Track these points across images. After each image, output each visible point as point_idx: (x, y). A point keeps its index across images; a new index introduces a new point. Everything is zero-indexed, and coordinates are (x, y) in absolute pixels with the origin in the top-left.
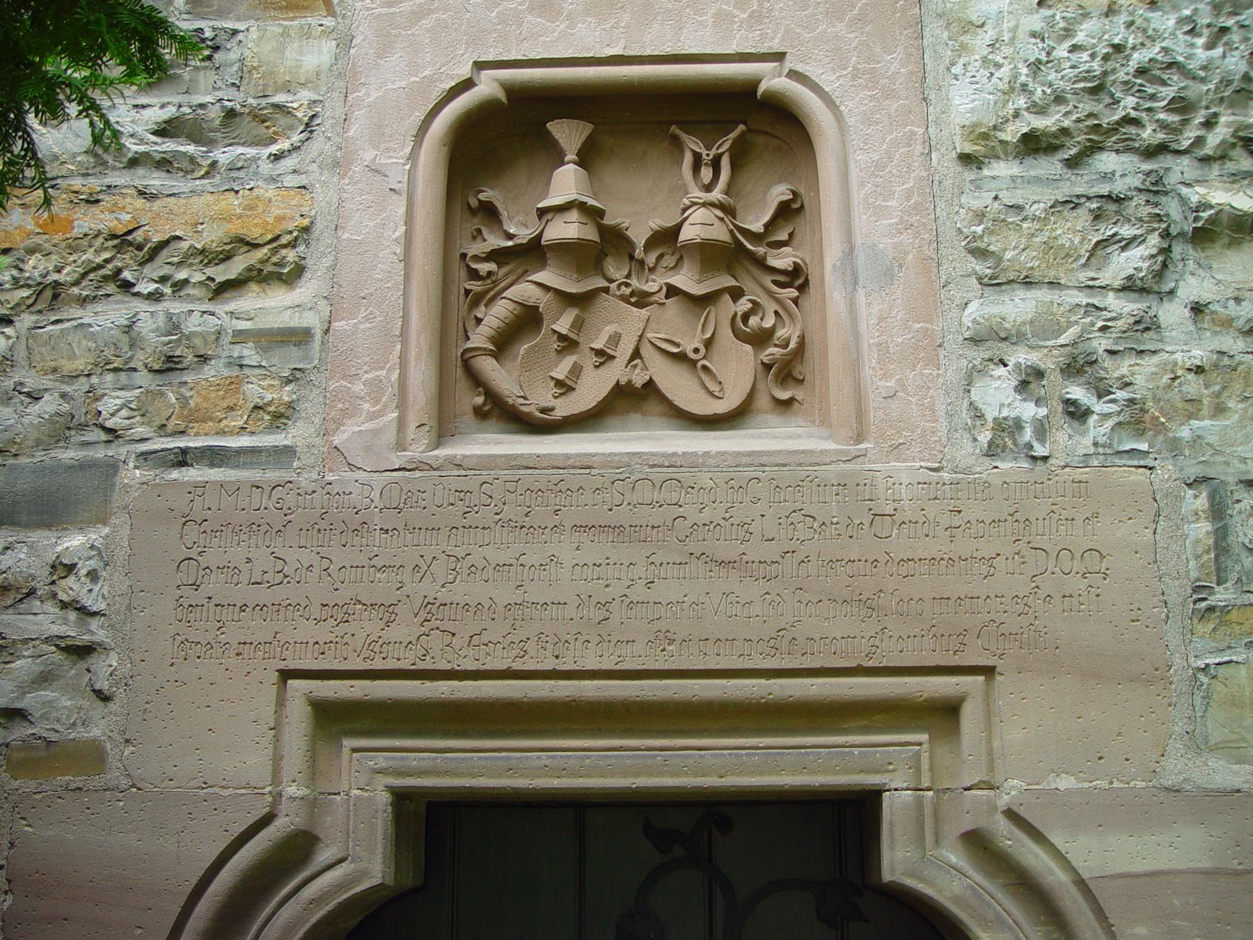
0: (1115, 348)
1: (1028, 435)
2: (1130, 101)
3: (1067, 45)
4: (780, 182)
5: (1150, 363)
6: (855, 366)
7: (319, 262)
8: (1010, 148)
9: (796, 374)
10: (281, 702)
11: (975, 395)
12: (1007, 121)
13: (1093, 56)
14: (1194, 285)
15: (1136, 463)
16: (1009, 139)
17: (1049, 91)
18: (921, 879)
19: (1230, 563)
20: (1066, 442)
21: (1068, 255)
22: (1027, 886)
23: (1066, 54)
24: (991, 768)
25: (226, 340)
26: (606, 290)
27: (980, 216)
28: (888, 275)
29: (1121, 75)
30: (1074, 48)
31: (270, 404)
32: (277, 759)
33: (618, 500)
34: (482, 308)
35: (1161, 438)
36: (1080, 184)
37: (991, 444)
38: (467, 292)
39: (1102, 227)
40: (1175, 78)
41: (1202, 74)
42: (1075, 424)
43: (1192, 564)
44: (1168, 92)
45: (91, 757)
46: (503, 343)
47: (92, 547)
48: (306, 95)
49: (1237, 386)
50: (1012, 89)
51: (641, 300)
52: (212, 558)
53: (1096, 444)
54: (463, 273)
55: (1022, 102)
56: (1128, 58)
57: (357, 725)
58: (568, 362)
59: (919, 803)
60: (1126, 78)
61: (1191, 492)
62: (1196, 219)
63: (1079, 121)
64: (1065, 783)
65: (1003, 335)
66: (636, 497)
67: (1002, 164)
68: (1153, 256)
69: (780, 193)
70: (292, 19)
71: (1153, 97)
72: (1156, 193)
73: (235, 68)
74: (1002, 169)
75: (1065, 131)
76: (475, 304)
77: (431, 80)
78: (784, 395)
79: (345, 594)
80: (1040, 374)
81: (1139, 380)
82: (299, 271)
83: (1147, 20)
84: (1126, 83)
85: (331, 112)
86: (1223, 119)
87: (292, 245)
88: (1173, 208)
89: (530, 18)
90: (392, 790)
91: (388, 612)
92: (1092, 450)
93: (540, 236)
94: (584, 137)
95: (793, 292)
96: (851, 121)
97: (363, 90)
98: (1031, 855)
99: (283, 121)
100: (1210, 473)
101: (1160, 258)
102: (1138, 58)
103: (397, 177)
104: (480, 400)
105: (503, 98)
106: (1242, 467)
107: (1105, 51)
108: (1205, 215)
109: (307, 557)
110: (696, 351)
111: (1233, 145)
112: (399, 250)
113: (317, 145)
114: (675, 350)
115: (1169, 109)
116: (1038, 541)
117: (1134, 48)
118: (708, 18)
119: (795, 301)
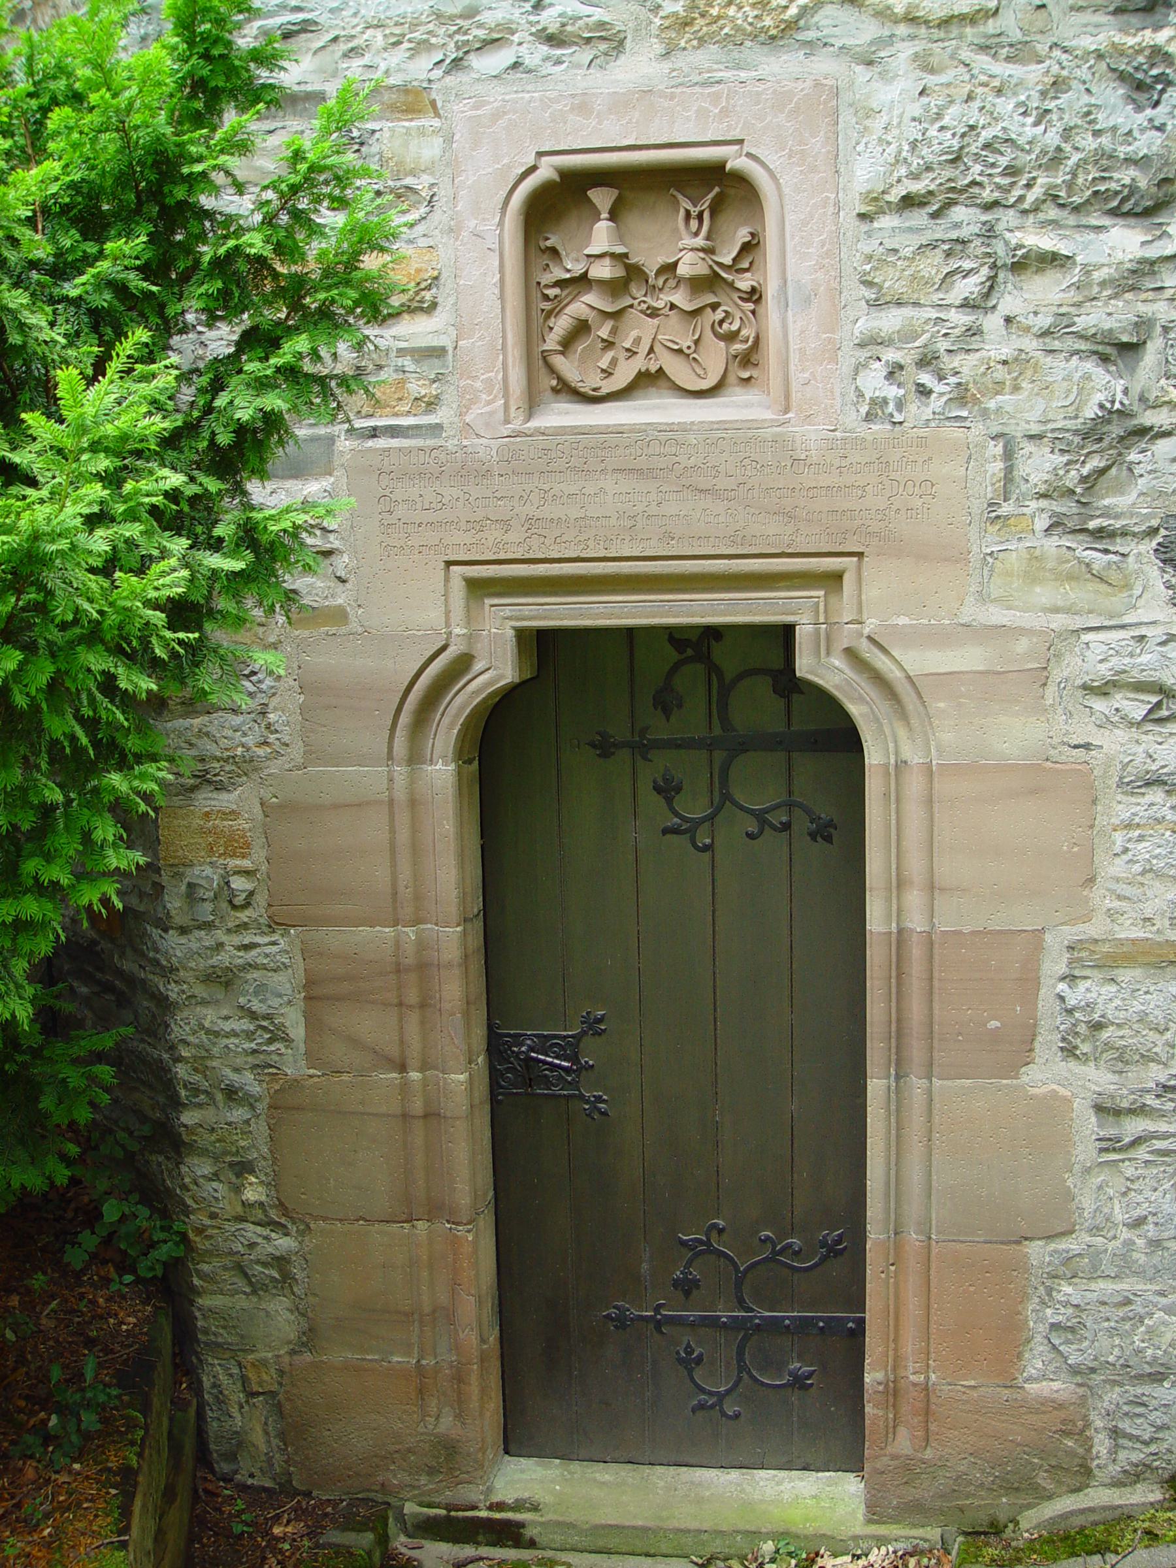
0: (952, 348)
1: (891, 407)
2: (978, 168)
3: (937, 125)
4: (745, 224)
5: (973, 358)
6: (785, 363)
7: (445, 296)
8: (893, 206)
9: (752, 360)
10: (447, 580)
11: (859, 382)
12: (892, 186)
13: (954, 135)
14: (1009, 302)
15: (958, 424)
16: (892, 200)
17: (922, 162)
18: (817, 676)
19: (1013, 488)
20: (917, 411)
21: (927, 283)
22: (878, 679)
23: (935, 133)
24: (860, 611)
25: (393, 354)
26: (631, 306)
27: (869, 258)
28: (807, 301)
29: (973, 149)
30: (942, 128)
31: (424, 396)
32: (447, 613)
33: (639, 452)
34: (553, 319)
35: (976, 408)
36: (940, 231)
37: (867, 414)
38: (543, 310)
39: (951, 261)
40: (1009, 150)
41: (1027, 147)
42: (923, 398)
43: (989, 488)
44: (1003, 161)
45: (339, 615)
46: (567, 343)
47: (325, 491)
48: (426, 179)
49: (1029, 373)
50: (897, 161)
51: (653, 313)
52: (398, 495)
53: (934, 413)
54: (539, 295)
55: (903, 171)
56: (978, 135)
57: (492, 590)
58: (610, 354)
59: (817, 631)
60: (976, 151)
61: (993, 443)
62: (1014, 256)
63: (941, 184)
64: (903, 621)
65: (879, 341)
66: (651, 451)
67: (887, 217)
68: (983, 283)
69: (743, 235)
70: (411, 120)
71: (993, 165)
72: (989, 237)
73: (377, 157)
74: (887, 222)
75: (930, 193)
76: (548, 317)
77: (509, 167)
78: (746, 375)
79: (480, 514)
80: (901, 367)
81: (965, 370)
82: (434, 305)
83: (994, 105)
84: (976, 154)
85: (443, 192)
86: (1039, 181)
87: (429, 288)
88: (999, 248)
89: (571, 117)
90: (516, 629)
91: (506, 525)
92: (931, 417)
93: (586, 272)
94: (614, 198)
95: (751, 306)
96: (786, 191)
97: (464, 174)
98: (881, 662)
99: (413, 198)
100: (1006, 430)
101: (988, 284)
102: (986, 135)
103: (492, 241)
104: (554, 382)
105: (558, 179)
106: (1027, 427)
107: (963, 130)
108: (1019, 253)
109: (456, 492)
110: (689, 348)
111: (1044, 201)
112: (497, 291)
113: (437, 216)
114: (676, 347)
115: (1004, 174)
116: (893, 476)
117: (983, 127)
118: (691, 113)
119: (753, 312)
